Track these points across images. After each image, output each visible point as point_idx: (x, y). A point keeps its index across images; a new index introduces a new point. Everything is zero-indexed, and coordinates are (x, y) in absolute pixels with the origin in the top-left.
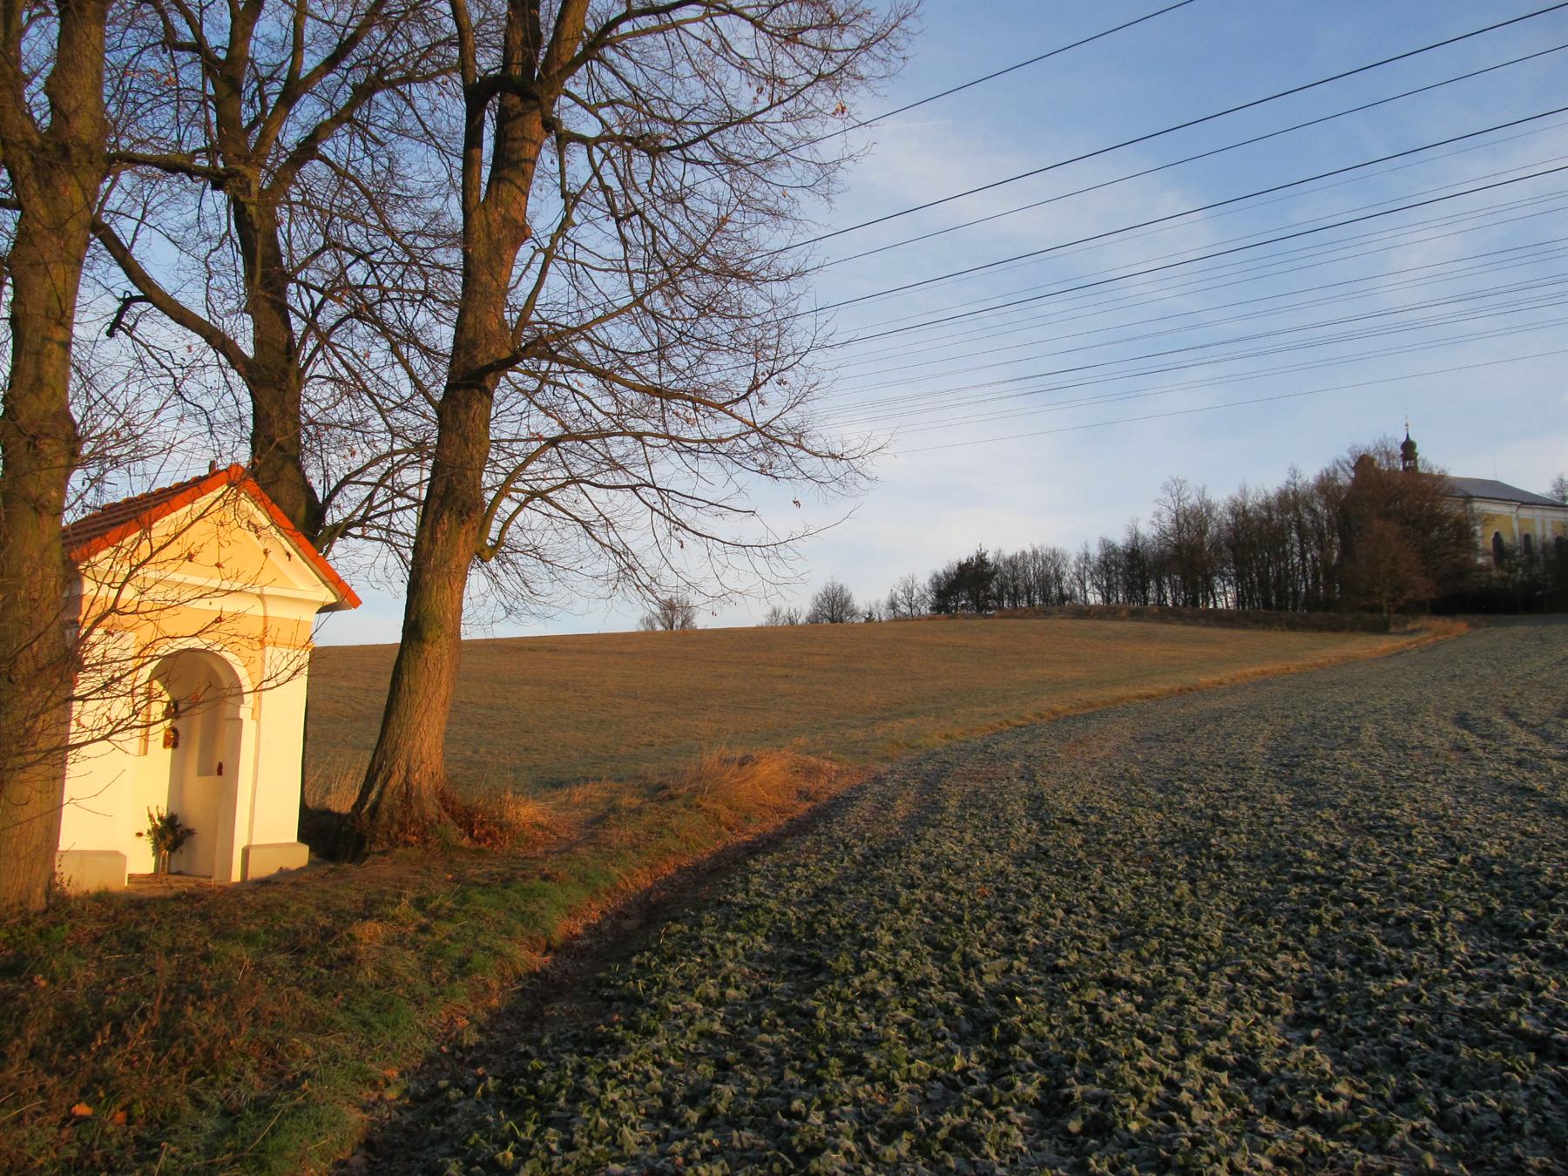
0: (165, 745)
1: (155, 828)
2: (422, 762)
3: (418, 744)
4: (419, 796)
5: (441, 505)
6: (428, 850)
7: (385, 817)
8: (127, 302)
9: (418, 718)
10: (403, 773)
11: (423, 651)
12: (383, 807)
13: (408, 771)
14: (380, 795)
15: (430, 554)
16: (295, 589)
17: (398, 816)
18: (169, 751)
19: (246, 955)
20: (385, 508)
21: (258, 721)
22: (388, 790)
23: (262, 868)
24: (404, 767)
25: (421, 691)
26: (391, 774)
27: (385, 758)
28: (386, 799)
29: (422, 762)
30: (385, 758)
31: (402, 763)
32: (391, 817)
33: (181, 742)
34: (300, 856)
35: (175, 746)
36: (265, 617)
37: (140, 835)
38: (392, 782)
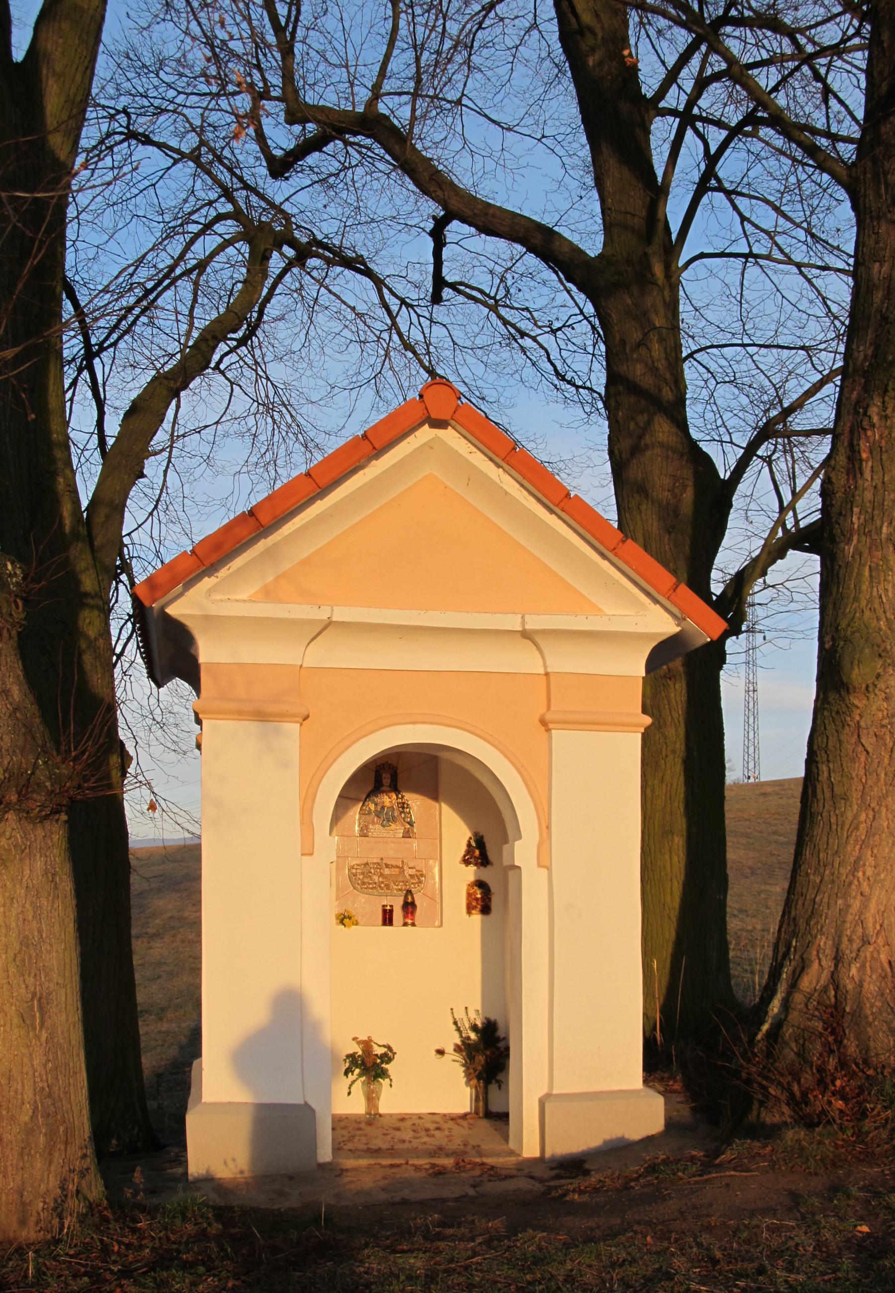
0: (470, 909)
1: (465, 1040)
2: (865, 941)
3: (856, 904)
4: (858, 1013)
5: (866, 389)
6: (860, 1135)
7: (789, 1053)
8: (202, 115)
9: (852, 850)
10: (828, 963)
11: (850, 707)
12: (788, 1032)
13: (838, 959)
14: (786, 1005)
15: (849, 501)
16: (599, 612)
17: (816, 1049)
18: (477, 917)
19: (843, 1150)
20: (194, 99)
21: (549, 868)
22: (798, 998)
23: (575, 1138)
24: (829, 952)
25: (855, 795)
26: (802, 967)
27: (794, 934)
28: (794, 1016)
29: (865, 941)
30: (794, 934)
31: (824, 942)
32: (801, 1054)
33: (495, 904)
34: (646, 1114)
35: (486, 910)
36: (547, 674)
37: (441, 1052)
38: (807, 982)
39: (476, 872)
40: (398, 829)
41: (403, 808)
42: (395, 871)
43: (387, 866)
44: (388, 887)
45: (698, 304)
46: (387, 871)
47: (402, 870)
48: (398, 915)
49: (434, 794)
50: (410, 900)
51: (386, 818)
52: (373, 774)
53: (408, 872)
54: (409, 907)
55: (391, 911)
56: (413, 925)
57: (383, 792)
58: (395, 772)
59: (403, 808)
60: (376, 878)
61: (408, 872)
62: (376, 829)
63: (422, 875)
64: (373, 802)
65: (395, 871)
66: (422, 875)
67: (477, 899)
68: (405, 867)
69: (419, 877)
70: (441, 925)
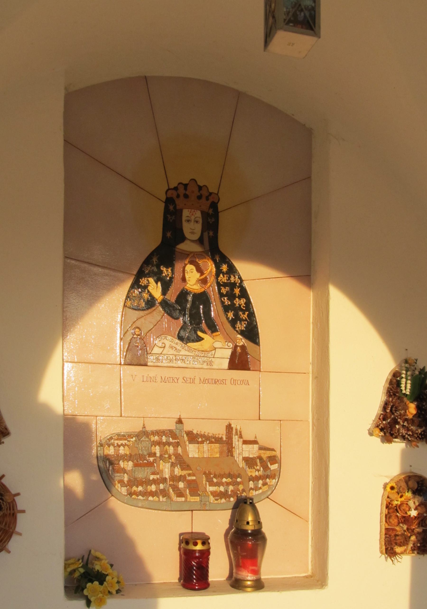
39: (404, 455)
40: (218, 348)
41: (231, 296)
42: (207, 450)
43: (193, 438)
44: (194, 491)
45: (194, 512)
46: (193, 451)
47: (226, 443)
48: (219, 566)
49: (303, 268)
50: (171, 207)
51: (192, 316)
52: (160, 208)
53: (243, 452)
54: (246, 543)
55: (205, 554)
56: (259, 585)
57: (185, 255)
58: (214, 206)
59: (231, 296)
60: (166, 469)
61: (243, 452)
62: (166, 346)
63: (273, 460)
64: (159, 279)
65: (207, 450)
66: (273, 460)
67: (406, 520)
68: (236, 441)
69: (267, 464)
70: (318, 579)
